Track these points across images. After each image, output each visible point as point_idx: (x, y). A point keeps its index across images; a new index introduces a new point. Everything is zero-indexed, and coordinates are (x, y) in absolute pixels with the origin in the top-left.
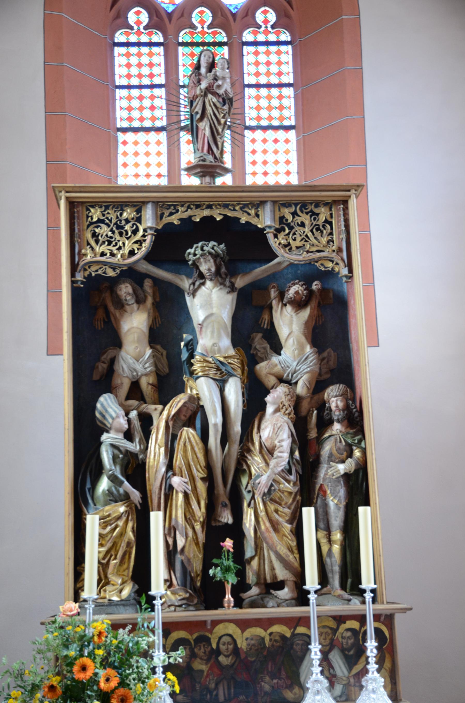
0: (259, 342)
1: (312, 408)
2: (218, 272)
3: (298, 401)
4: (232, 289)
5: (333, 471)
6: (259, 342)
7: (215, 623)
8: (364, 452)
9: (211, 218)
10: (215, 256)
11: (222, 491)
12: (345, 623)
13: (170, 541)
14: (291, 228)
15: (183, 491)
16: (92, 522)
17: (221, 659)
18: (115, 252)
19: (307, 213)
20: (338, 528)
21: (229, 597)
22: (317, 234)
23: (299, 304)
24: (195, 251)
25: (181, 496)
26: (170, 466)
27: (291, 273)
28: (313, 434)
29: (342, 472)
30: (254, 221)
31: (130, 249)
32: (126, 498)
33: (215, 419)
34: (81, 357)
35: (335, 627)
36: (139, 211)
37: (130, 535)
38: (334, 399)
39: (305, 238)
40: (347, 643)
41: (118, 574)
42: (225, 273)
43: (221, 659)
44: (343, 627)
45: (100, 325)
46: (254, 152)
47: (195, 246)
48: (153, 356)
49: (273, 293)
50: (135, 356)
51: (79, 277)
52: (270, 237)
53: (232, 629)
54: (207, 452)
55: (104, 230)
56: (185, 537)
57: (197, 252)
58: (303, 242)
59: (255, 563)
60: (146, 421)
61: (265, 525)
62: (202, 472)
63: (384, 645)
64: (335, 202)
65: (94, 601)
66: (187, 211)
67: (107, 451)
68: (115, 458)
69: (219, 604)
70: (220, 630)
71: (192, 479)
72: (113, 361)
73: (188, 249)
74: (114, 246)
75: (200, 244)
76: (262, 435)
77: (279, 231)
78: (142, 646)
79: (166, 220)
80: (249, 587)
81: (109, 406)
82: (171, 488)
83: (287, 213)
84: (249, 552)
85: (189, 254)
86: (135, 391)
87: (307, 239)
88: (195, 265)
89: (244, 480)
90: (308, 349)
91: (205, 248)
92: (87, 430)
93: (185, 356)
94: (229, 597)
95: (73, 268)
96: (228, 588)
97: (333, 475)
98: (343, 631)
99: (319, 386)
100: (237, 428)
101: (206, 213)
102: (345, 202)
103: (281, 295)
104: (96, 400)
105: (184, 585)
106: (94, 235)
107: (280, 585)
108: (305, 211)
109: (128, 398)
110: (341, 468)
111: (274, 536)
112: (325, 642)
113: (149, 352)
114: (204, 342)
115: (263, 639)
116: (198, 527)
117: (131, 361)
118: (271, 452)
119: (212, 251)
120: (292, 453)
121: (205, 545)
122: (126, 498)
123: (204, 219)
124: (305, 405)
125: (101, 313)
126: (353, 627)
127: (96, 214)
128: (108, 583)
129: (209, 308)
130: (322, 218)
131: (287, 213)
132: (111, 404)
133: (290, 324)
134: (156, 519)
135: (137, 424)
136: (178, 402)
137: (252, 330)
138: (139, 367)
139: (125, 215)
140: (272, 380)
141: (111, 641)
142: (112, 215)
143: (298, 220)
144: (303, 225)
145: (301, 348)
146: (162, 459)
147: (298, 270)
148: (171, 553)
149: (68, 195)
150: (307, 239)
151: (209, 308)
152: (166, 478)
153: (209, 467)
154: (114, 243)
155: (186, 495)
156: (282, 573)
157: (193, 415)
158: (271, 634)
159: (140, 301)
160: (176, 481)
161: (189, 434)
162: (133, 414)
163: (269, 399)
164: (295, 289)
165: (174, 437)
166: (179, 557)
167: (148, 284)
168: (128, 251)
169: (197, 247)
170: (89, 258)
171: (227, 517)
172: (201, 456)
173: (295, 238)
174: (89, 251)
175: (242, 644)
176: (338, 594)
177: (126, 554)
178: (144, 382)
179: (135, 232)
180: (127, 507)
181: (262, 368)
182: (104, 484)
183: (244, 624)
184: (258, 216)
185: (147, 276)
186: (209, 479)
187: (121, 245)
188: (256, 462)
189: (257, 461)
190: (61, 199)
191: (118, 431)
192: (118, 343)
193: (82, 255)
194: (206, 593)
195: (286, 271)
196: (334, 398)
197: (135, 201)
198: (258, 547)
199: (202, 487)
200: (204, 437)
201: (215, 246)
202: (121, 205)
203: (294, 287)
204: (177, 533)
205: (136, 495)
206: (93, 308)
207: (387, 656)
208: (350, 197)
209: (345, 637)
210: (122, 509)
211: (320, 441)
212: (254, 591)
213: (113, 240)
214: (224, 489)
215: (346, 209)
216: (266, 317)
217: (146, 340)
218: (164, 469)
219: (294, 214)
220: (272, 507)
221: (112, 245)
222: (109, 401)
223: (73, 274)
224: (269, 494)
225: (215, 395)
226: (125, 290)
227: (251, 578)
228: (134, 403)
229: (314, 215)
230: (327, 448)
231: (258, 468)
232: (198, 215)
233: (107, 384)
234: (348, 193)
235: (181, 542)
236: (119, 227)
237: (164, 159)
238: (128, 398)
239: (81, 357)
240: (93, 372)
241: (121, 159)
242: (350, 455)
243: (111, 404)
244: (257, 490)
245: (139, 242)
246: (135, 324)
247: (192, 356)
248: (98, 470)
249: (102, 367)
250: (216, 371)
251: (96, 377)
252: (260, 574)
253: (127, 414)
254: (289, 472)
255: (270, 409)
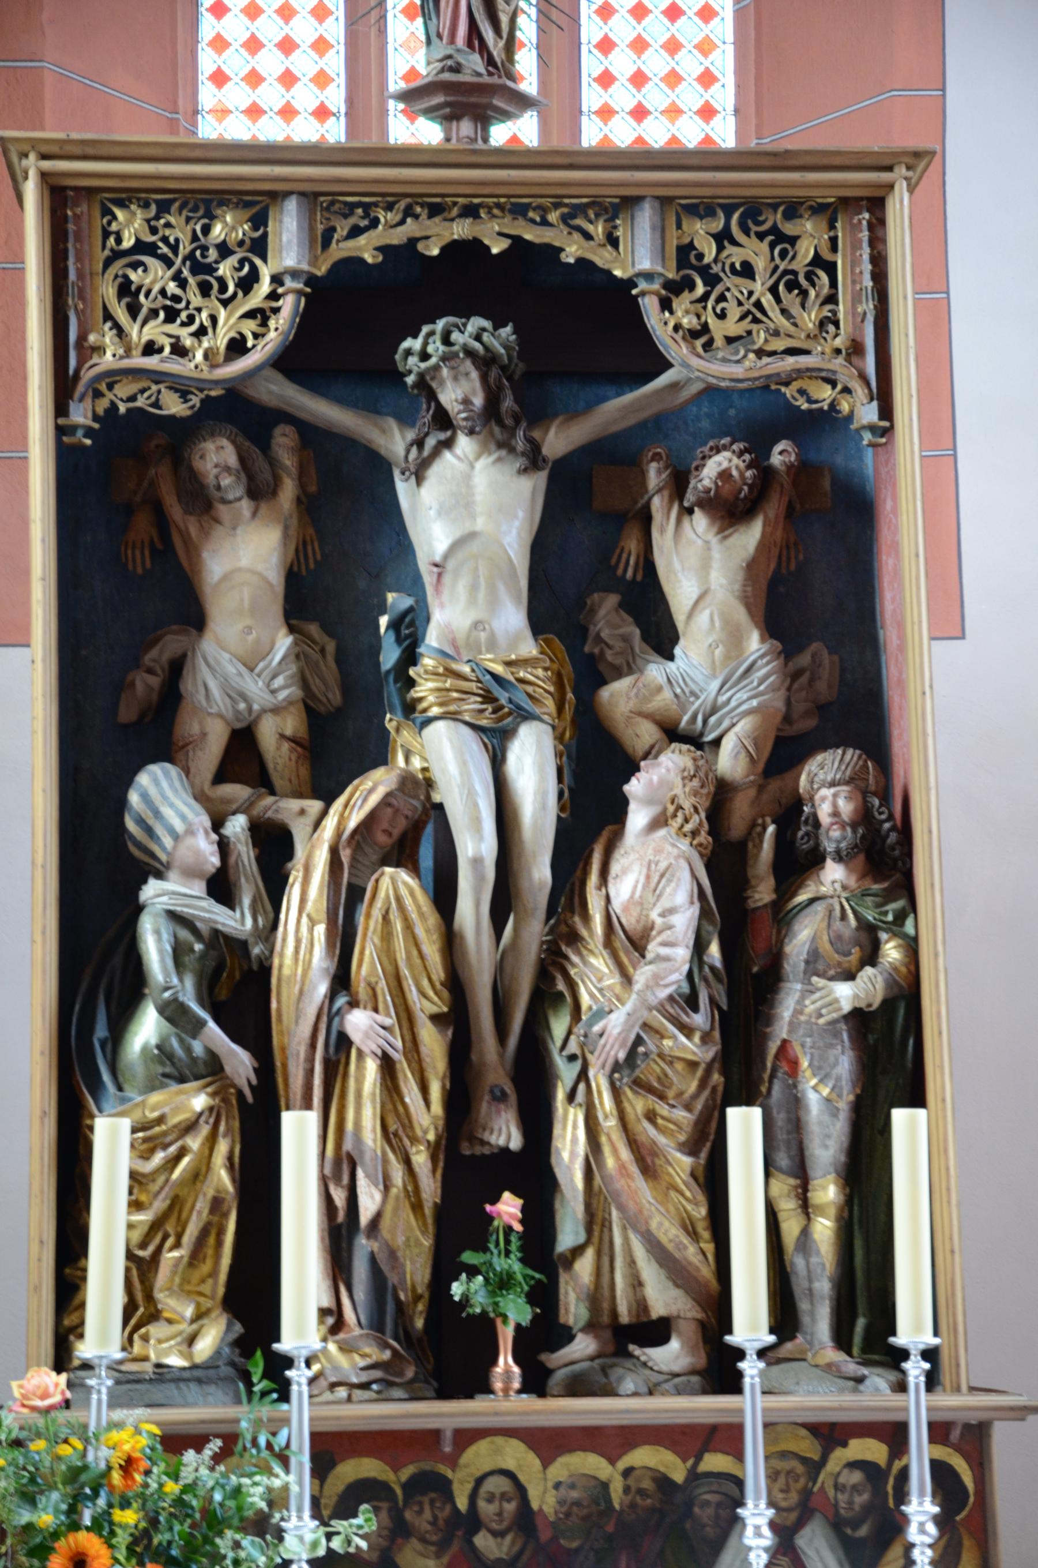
0: (610, 621)
1: (763, 816)
2: (491, 411)
3: (720, 796)
4: (534, 460)
5: (818, 1005)
6: (610, 621)
7: (466, 1437)
8: (912, 947)
9: (475, 247)
10: (485, 362)
11: (493, 1056)
12: (845, 1445)
13: (339, 1197)
14: (712, 281)
15: (379, 1053)
16: (111, 1138)
17: (483, 1541)
18: (188, 342)
19: (761, 236)
20: (832, 1170)
21: (506, 1364)
22: (791, 299)
23: (730, 510)
24: (425, 344)
25: (372, 1067)
26: (341, 980)
27: (708, 416)
28: (763, 893)
29: (846, 1007)
30: (603, 257)
31: (232, 335)
32: (212, 1068)
33: (475, 844)
34: (84, 652)
35: (816, 1457)
36: (259, 221)
37: (222, 1178)
38: (826, 792)
39: (754, 310)
40: (851, 1503)
41: (185, 1290)
42: (512, 413)
43: (483, 1541)
44: (840, 1456)
45: (140, 561)
46: (606, 45)
47: (425, 329)
48: (297, 655)
49: (654, 476)
50: (245, 656)
51: (80, 415)
52: (650, 306)
53: (515, 1455)
54: (451, 940)
55: (154, 276)
56: (381, 1187)
57: (430, 349)
58: (746, 324)
59: (585, 1266)
60: (274, 847)
61: (616, 1155)
62: (436, 999)
63: (959, 1514)
64: (847, 204)
65: (114, 1367)
66: (402, 222)
67: (157, 932)
68: (179, 953)
69: (478, 1384)
70: (480, 1457)
71: (406, 1016)
72: (177, 668)
73: (404, 339)
74: (183, 324)
75: (440, 324)
76: (612, 894)
77: (676, 287)
78: (250, 1500)
79: (341, 249)
80: (567, 1336)
81: (164, 801)
82: (344, 1042)
83: (701, 233)
84: (569, 1233)
85: (408, 352)
86: (242, 757)
87: (759, 315)
88: (426, 388)
89: (559, 1026)
90: (754, 643)
91: (455, 336)
92: (98, 872)
93: (390, 656)
94: (506, 1364)
95: (63, 388)
96: (506, 1335)
97: (821, 1016)
98: (837, 1469)
99: (784, 752)
100: (539, 872)
101: (461, 230)
102: (876, 204)
103: (679, 482)
104: (127, 781)
105: (377, 1325)
106: (125, 289)
107: (657, 1332)
108: (754, 228)
109: (220, 777)
110: (845, 994)
111: (641, 1191)
112: (785, 1499)
113: (284, 642)
114: (448, 618)
115: (605, 1486)
116: (421, 1159)
117: (231, 668)
118: (638, 944)
119: (477, 345)
120: (699, 947)
121: (441, 1213)
122: (212, 1068)
123: (452, 248)
124: (741, 809)
125: (143, 526)
126: (869, 1457)
127: (131, 226)
128: (154, 1316)
129: (465, 514)
130: (806, 251)
131: (701, 233)
132: (169, 793)
133: (701, 567)
134: (299, 1132)
135: (245, 853)
136: (368, 793)
137: (589, 587)
138: (255, 688)
139: (218, 231)
140: (647, 733)
141: (161, 1485)
142: (180, 230)
143: (735, 255)
144: (747, 271)
145: (734, 640)
146: (320, 958)
147: (731, 407)
148: (340, 1233)
149: (47, 165)
150: (759, 315)
151: (465, 514)
152: (330, 1014)
153: (456, 985)
154: (184, 315)
155: (387, 1065)
156: (662, 1298)
157: (414, 832)
158: (627, 1472)
159: (259, 492)
160: (358, 1022)
161: (398, 886)
162: (237, 825)
163: (634, 787)
164: (719, 465)
165: (356, 895)
166: (363, 1246)
167: (284, 442)
168: (225, 341)
169: (432, 333)
170: (108, 360)
171: (506, 1133)
172: (432, 951)
173: (723, 310)
174: (109, 338)
175: (543, 1499)
176: (827, 1360)
177: (210, 1231)
178: (268, 733)
179: (247, 284)
180: (213, 1095)
181: (618, 696)
182: (147, 1029)
183: (549, 1442)
184: (613, 241)
185: (283, 416)
186: (456, 1019)
187: (207, 323)
188: (593, 972)
189: (597, 969)
190: (26, 178)
191: (190, 873)
192: (194, 617)
193: (88, 351)
194: (442, 1350)
195: (695, 409)
196: (827, 787)
197: (248, 188)
198: (595, 1221)
199: (434, 1044)
200: (444, 895)
201: (484, 330)
202: (205, 202)
203: (718, 458)
204: (360, 1173)
205: (240, 1062)
206: (124, 504)
207: (967, 1542)
208: (891, 187)
209: (844, 1486)
210: (200, 1102)
211: (782, 916)
212: (583, 1346)
213: (183, 305)
214: (501, 1050)
215: (878, 225)
216: (632, 545)
217: (275, 609)
218: (322, 988)
219: (723, 238)
220: (637, 1104)
221: (178, 321)
222: (165, 784)
223: (61, 408)
224: (629, 1066)
225: (478, 775)
226: (217, 457)
227: (573, 1309)
228: (237, 791)
229: (782, 241)
230: (804, 936)
231: (600, 990)
232: (435, 238)
233: (158, 735)
234: (885, 177)
235: (369, 1201)
236: (198, 268)
237: (335, 62)
238: (220, 777)
239: (84, 652)
240: (115, 711)
241: (207, 61)
242: (871, 957)
243: (169, 793)
244: (596, 1054)
245: (261, 315)
246: (245, 558)
247: (410, 657)
248: (130, 988)
249: (145, 684)
250: (482, 703)
251: (127, 713)
252: (598, 1298)
253: (217, 825)
254: (692, 1002)
255: (637, 818)
